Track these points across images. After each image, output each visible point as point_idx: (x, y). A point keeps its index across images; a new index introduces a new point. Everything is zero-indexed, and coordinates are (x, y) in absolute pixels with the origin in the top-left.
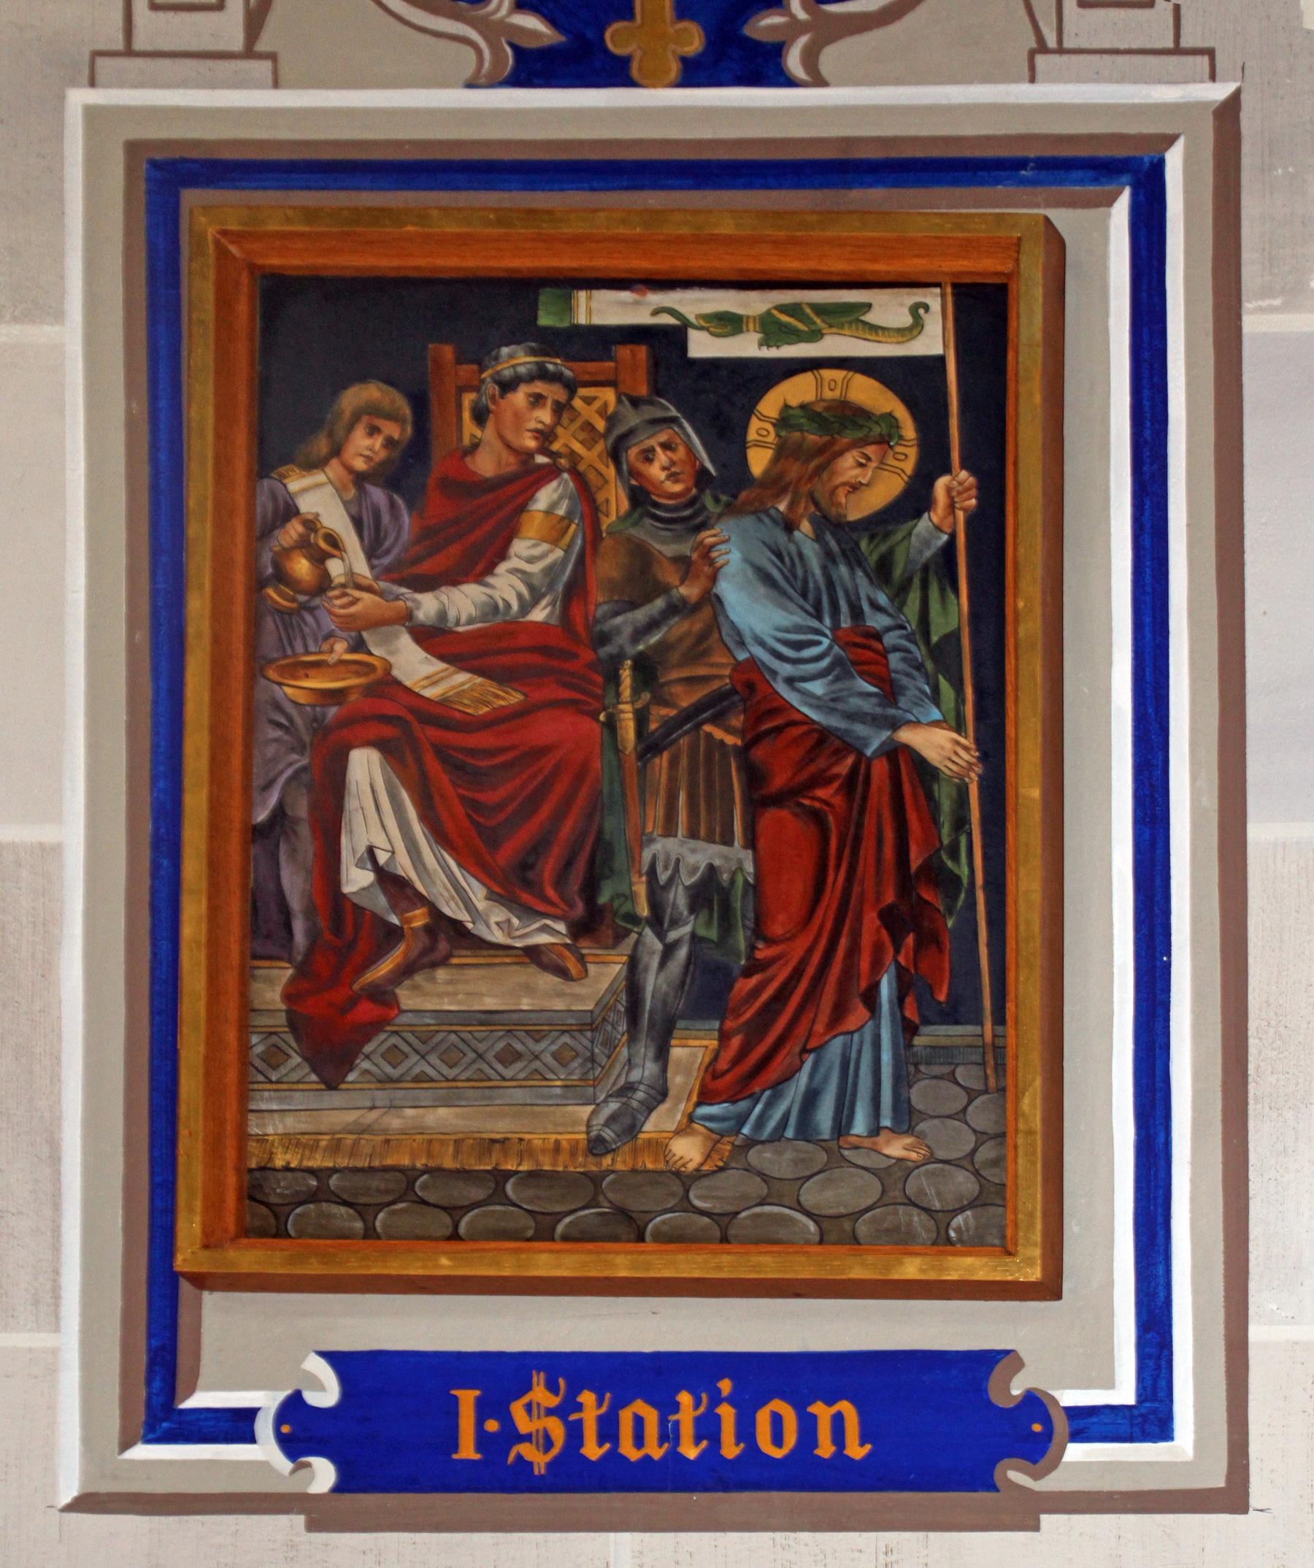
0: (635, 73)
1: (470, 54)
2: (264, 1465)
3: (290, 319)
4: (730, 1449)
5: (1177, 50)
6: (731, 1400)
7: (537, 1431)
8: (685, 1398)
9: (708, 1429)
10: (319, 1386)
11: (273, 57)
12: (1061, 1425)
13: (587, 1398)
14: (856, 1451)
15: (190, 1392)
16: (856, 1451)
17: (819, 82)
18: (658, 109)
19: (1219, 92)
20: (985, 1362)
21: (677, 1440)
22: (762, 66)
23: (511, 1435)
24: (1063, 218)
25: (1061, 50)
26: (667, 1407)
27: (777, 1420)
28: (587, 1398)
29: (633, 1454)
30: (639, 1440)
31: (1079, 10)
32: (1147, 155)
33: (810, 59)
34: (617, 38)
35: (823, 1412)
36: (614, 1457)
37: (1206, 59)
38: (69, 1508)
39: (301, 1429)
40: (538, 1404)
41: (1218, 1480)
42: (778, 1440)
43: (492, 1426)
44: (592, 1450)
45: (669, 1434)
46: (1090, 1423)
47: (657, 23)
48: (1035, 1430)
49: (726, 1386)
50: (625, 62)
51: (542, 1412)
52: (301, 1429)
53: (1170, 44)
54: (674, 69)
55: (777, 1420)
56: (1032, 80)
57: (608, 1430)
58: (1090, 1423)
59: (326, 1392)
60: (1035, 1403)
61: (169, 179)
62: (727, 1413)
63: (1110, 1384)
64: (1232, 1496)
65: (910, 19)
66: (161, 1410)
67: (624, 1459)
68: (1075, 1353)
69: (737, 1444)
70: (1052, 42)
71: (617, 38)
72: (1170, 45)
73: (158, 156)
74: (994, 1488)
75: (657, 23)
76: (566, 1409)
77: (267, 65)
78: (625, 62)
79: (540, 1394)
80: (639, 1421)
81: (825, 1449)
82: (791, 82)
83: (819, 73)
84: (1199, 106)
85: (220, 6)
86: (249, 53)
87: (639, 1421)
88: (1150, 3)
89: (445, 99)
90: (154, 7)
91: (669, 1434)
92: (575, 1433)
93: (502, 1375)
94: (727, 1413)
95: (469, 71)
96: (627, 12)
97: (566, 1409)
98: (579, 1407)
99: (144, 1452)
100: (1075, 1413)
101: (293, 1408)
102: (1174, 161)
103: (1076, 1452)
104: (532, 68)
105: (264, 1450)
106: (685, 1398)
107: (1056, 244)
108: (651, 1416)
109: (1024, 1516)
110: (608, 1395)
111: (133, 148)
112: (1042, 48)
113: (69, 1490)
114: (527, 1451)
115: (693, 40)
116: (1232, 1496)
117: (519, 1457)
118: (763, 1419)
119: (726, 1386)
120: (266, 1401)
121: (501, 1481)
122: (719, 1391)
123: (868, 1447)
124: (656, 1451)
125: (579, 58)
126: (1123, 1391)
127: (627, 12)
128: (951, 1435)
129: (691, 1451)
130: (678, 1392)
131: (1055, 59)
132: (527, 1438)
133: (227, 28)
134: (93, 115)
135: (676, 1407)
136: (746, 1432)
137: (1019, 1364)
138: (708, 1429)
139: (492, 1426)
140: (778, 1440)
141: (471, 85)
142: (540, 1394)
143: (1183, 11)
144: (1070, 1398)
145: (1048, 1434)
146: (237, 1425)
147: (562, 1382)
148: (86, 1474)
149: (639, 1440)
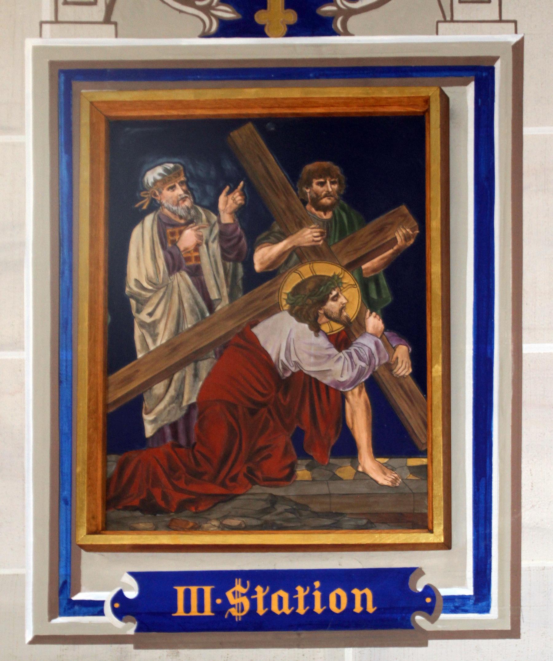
0: (266, 31)
1: (201, 24)
2: (109, 624)
3: (122, 139)
4: (318, 609)
5: (501, 21)
6: (320, 589)
7: (238, 604)
8: (300, 589)
9: (309, 600)
10: (131, 589)
11: (116, 24)
12: (439, 604)
13: (259, 589)
14: (371, 609)
15: (78, 591)
16: (371, 609)
17: (347, 33)
18: (276, 46)
19: (514, 39)
20: (411, 570)
21: (296, 607)
22: (324, 27)
23: (227, 604)
24: (448, 90)
25: (452, 21)
26: (292, 592)
27: (338, 597)
28: (259, 589)
29: (278, 612)
30: (280, 606)
31: (516, 19)
32: (486, 64)
33: (344, 23)
34: (260, 17)
35: (357, 593)
36: (270, 613)
37: (513, 25)
38: (31, 642)
39: (123, 607)
40: (238, 592)
41: (507, 626)
42: (338, 605)
43: (219, 601)
44: (261, 610)
45: (293, 603)
46: (456, 604)
47: (276, 11)
48: (428, 603)
49: (317, 584)
50: (263, 27)
51: (240, 595)
52: (123, 607)
53: (498, 19)
54: (284, 30)
55: (338, 597)
56: (437, 33)
57: (267, 601)
58: (456, 604)
59: (132, 593)
60: (429, 590)
61: (69, 78)
62: (317, 595)
63: (463, 584)
64: (514, 632)
65: (387, 7)
66: (63, 597)
67: (274, 614)
68: (447, 573)
69: (374, 607)
70: (448, 18)
71: (260, 17)
72: (498, 19)
73: (63, 68)
74: (412, 628)
75: (276, 11)
76: (251, 593)
77: (113, 27)
78: (263, 27)
79: (238, 588)
80: (280, 599)
81: (358, 609)
82: (334, 33)
83: (347, 31)
84: (507, 43)
85: (95, 3)
86: (107, 20)
87: (280, 599)
88: (489, 1)
89: (189, 41)
90: (460, 2)
91: (293, 603)
92: (254, 603)
93: (222, 580)
94: (317, 595)
95: (200, 30)
96: (264, 6)
97: (251, 593)
98: (255, 593)
99: (61, 620)
100: (449, 599)
101: (119, 597)
102: (498, 66)
103: (443, 616)
104: (226, 29)
105: (109, 617)
106: (300, 589)
107: (445, 100)
108: (285, 595)
109: (422, 639)
110: (268, 588)
111: (52, 64)
112: (445, 21)
113: (29, 637)
114: (234, 612)
115: (292, 17)
116: (514, 632)
117: (230, 614)
118: (332, 598)
119: (317, 584)
120: (107, 596)
121: (219, 625)
122: (314, 586)
123: (375, 608)
124: (287, 610)
125: (245, 27)
126: (467, 589)
127: (264, 6)
128: (396, 607)
129: (301, 610)
130: (296, 586)
131: (452, 24)
132: (234, 606)
133: (98, 12)
134: (37, 50)
135: (296, 593)
136: (325, 601)
137: (422, 573)
138: (309, 600)
139: (219, 601)
140: (338, 605)
141: (205, 35)
142: (238, 588)
143: (514, 31)
144: (444, 592)
145: (115, 600)
146: (94, 608)
147: (248, 582)
148: (35, 630)
149: (280, 606)
